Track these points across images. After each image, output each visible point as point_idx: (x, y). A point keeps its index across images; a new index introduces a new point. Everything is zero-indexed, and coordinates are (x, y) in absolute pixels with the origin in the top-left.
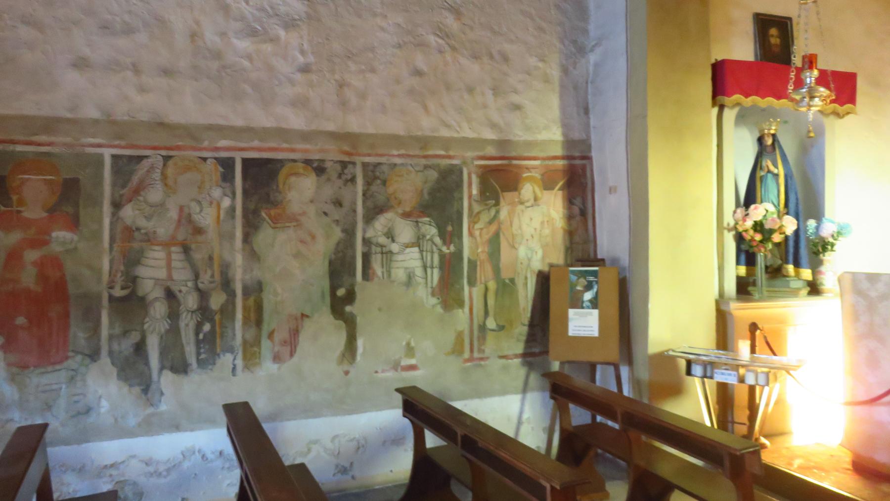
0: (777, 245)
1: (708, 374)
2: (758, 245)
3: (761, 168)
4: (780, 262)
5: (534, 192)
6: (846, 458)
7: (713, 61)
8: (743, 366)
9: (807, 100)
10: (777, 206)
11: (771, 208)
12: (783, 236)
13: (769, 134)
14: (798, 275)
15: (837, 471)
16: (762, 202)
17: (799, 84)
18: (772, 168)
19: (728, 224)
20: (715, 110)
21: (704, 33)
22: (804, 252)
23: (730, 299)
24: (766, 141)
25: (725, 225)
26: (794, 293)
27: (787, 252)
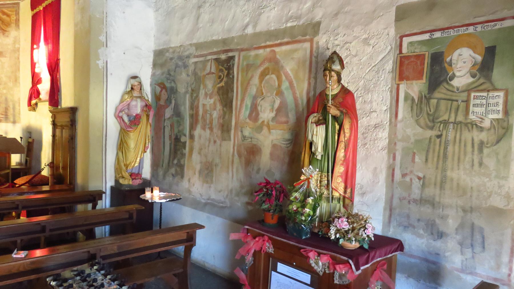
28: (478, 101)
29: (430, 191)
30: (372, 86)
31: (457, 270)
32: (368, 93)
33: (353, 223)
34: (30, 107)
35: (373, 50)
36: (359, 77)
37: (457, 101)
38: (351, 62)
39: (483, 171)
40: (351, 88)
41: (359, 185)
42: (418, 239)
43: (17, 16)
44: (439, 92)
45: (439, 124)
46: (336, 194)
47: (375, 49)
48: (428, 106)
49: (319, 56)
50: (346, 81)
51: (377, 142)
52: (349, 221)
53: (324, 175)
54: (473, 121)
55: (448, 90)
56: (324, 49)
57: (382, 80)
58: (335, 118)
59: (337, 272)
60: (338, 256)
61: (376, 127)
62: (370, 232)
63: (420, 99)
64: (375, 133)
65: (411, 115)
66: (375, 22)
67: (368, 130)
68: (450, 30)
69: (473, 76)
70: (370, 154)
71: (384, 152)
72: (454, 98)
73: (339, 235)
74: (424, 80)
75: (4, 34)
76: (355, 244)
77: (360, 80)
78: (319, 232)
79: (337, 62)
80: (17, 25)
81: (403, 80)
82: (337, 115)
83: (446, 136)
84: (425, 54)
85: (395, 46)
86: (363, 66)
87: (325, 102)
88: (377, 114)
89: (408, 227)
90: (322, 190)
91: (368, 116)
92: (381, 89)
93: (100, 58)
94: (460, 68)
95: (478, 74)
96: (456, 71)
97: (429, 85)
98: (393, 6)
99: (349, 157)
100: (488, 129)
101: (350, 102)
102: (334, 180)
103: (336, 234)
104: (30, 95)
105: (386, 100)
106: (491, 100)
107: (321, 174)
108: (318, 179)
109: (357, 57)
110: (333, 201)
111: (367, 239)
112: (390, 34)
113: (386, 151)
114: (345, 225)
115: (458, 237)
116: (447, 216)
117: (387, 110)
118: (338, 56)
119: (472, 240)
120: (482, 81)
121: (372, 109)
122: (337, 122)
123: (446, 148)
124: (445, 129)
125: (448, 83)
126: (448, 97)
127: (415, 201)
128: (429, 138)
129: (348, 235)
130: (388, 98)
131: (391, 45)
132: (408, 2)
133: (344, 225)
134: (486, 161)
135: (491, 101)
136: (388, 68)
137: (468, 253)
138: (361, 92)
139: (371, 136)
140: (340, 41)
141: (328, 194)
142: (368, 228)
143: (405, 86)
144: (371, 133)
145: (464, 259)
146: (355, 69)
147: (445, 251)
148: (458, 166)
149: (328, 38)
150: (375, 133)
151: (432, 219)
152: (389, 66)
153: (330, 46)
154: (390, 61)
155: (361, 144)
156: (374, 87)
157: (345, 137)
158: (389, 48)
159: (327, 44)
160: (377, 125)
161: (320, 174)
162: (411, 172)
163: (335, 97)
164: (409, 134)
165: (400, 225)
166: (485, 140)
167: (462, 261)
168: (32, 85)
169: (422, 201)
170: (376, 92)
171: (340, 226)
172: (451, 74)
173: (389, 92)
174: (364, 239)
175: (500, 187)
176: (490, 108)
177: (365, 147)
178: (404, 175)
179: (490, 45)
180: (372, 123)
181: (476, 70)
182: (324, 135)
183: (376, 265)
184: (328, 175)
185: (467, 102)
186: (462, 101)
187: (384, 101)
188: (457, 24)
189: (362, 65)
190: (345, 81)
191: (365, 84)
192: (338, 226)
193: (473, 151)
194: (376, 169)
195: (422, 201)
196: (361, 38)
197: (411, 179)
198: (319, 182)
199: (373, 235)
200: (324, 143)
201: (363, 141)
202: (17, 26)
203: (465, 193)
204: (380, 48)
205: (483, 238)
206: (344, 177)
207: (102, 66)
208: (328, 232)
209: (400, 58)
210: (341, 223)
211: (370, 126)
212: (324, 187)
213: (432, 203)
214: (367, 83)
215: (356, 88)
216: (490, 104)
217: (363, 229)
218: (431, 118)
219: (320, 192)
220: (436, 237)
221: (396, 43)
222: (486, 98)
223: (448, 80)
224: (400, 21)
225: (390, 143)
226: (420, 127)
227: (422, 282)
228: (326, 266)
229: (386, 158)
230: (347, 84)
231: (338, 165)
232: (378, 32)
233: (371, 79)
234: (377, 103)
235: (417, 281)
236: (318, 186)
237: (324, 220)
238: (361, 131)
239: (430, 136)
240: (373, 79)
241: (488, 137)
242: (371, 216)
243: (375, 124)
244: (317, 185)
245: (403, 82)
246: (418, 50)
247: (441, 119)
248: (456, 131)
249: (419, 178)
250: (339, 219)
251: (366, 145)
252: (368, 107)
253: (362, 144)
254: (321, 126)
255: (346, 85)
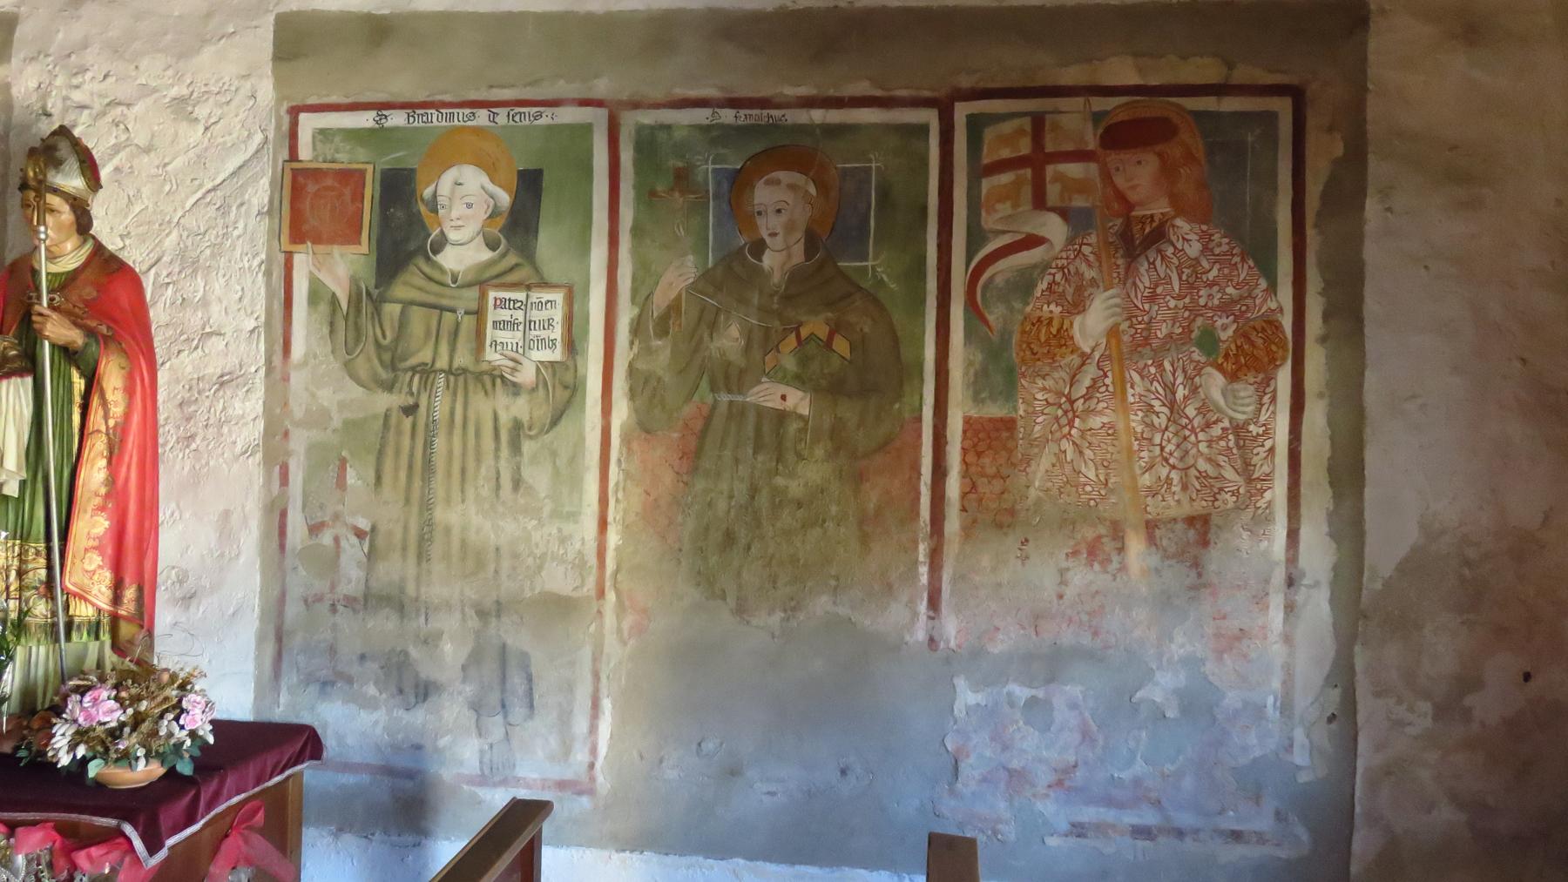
28: (505, 315)
29: (392, 570)
30: (208, 252)
31: (471, 781)
32: (195, 271)
33: (137, 699)
35: (206, 140)
36: (163, 220)
37: (453, 311)
38: (131, 167)
39: (522, 501)
40: (134, 257)
41: (174, 572)
42: (363, 714)
44: (406, 283)
45: (410, 374)
46: (83, 611)
47: (214, 135)
48: (377, 320)
49: (11, 134)
50: (115, 231)
51: (230, 431)
52: (124, 694)
53: (35, 548)
54: (494, 369)
55: (430, 279)
56: (31, 114)
57: (239, 237)
58: (66, 353)
59: (84, 875)
60: (85, 818)
61: (222, 384)
62: (198, 720)
63: (355, 300)
64: (222, 401)
65: (329, 348)
66: (208, 53)
67: (199, 393)
68: (429, 111)
69: (492, 245)
70: (205, 470)
71: (251, 459)
72: (445, 302)
73: (86, 749)
74: (364, 248)
76: (149, 768)
77: (167, 231)
78: (17, 748)
79: (72, 164)
81: (302, 241)
82: (75, 342)
83: (428, 410)
84: (366, 170)
85: (275, 136)
86: (175, 187)
87: (30, 298)
88: (225, 343)
89: (333, 684)
90: (27, 602)
91: (196, 348)
92: (235, 263)
94: (458, 219)
95: (503, 241)
96: (449, 228)
97: (377, 259)
98: (268, 11)
99: (127, 480)
100: (530, 388)
101: (124, 302)
102: (73, 563)
103: (72, 747)
105: (253, 299)
106: (534, 312)
107: (21, 546)
108: (12, 565)
109: (152, 154)
110: (74, 636)
111: (188, 742)
112: (259, 96)
113: (259, 456)
114: (108, 712)
115: (468, 689)
116: (439, 635)
117: (256, 331)
118: (76, 145)
119: (503, 691)
120: (512, 259)
121: (207, 327)
122: (78, 368)
123: (428, 444)
124: (426, 390)
125: (428, 259)
126: (431, 299)
127: (350, 602)
128: (383, 414)
129: (117, 744)
130: (259, 295)
131: (265, 130)
132: (311, 8)
133: (104, 713)
134: (526, 473)
135: (536, 315)
136: (255, 201)
137: (496, 726)
138: (170, 270)
139: (209, 412)
140: (92, 94)
141: (54, 614)
142: (190, 708)
143: (310, 259)
144: (207, 404)
145: (487, 747)
146: (146, 191)
147: (436, 736)
148: (463, 491)
149: (45, 78)
150: (222, 401)
151: (399, 649)
152: (260, 193)
153: (55, 105)
154: (262, 178)
155: (175, 438)
156: (213, 255)
157: (106, 417)
158: (259, 138)
159: (45, 97)
160: (225, 378)
161: (17, 548)
162: (336, 517)
163: (65, 283)
164: (325, 404)
165: (309, 679)
166: (525, 419)
167: (482, 752)
169: (370, 600)
170: (221, 272)
171: (88, 717)
172: (436, 236)
173: (260, 275)
174: (181, 744)
175: (563, 540)
176: (533, 332)
177: (188, 446)
178: (315, 529)
179: (531, 167)
180: (210, 370)
181: (499, 228)
182: (28, 411)
183: (228, 820)
184: (49, 550)
185: (479, 313)
186: (467, 313)
187: (246, 301)
188: (448, 98)
189: (171, 181)
190: (112, 228)
191: (184, 243)
192: (81, 720)
193: (497, 449)
194: (226, 514)
195: (370, 600)
196: (165, 96)
197: (337, 540)
198: (13, 574)
199: (211, 727)
200: (30, 438)
201: (182, 428)
203: (480, 564)
204: (230, 134)
205: (530, 679)
206: (109, 551)
208: (47, 745)
209: (293, 173)
210: (93, 707)
211: (205, 381)
212: (33, 591)
213: (396, 602)
214: (189, 242)
215: (151, 255)
216: (532, 324)
217: (170, 716)
218: (387, 357)
219: (20, 611)
220: (412, 700)
221: (278, 127)
222: (524, 307)
223: (430, 254)
224: (289, 60)
225: (268, 433)
226: (358, 384)
227: (378, 836)
228: (43, 862)
229: (258, 480)
230: (122, 240)
231: (85, 511)
232: (221, 85)
233: (202, 230)
234: (224, 307)
235: (366, 837)
236: (12, 588)
237: (43, 702)
238: (175, 396)
239: (385, 407)
240: (210, 231)
241: (531, 409)
242: (204, 667)
243: (218, 375)
244: (7, 588)
245: (301, 247)
246: (346, 157)
247: (413, 361)
248: (455, 394)
249: (360, 534)
250: (83, 695)
251: (194, 440)
252: (195, 319)
253: (178, 438)
254: (15, 380)
255: (112, 244)
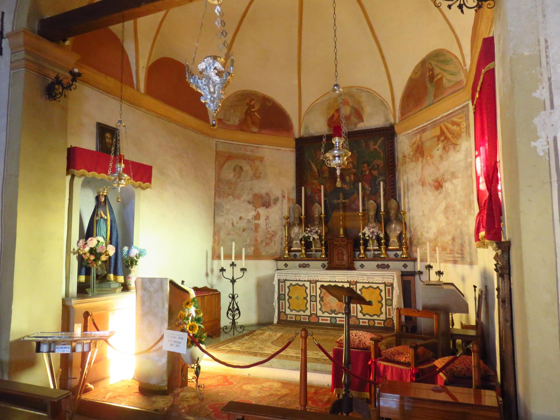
0: (105, 262)
1: (52, 350)
2: (92, 262)
3: (97, 215)
4: (106, 272)
5: (453, 82)
6: (136, 386)
7: (69, 146)
8: (75, 341)
9: (117, 180)
10: (105, 239)
11: (101, 239)
12: (108, 257)
13: (103, 195)
14: (116, 280)
15: (131, 395)
16: (96, 236)
17: (114, 170)
18: (103, 215)
19: (74, 249)
20: (69, 177)
21: (64, 128)
22: (120, 265)
23: (73, 298)
24: (101, 199)
25: (72, 250)
26: (113, 291)
27: (110, 266)
34: (478, 242)
43: (467, 121)
75: (455, 149)
80: (468, 133)
93: (539, 134)
104: (477, 225)
168: (480, 209)
202: (468, 135)
207: (544, 151)
